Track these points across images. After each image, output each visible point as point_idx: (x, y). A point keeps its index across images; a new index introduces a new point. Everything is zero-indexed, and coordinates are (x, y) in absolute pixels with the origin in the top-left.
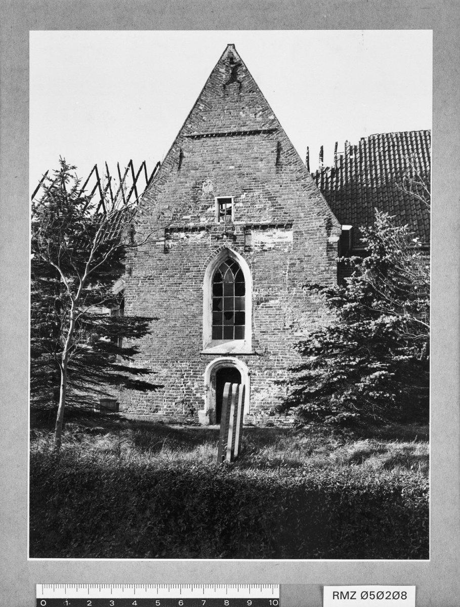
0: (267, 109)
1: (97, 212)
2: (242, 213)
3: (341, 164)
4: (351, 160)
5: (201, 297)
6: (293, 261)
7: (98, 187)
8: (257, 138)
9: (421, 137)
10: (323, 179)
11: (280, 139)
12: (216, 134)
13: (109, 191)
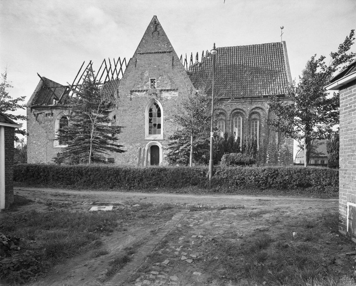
0: (169, 43)
1: (105, 80)
2: (159, 85)
3: (204, 61)
4: (208, 59)
5: (144, 118)
6: (178, 104)
7: (106, 69)
8: (165, 54)
9: (236, 49)
10: (196, 67)
11: (174, 55)
12: (149, 53)
13: (110, 70)
